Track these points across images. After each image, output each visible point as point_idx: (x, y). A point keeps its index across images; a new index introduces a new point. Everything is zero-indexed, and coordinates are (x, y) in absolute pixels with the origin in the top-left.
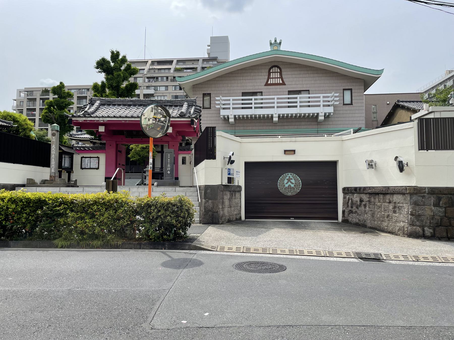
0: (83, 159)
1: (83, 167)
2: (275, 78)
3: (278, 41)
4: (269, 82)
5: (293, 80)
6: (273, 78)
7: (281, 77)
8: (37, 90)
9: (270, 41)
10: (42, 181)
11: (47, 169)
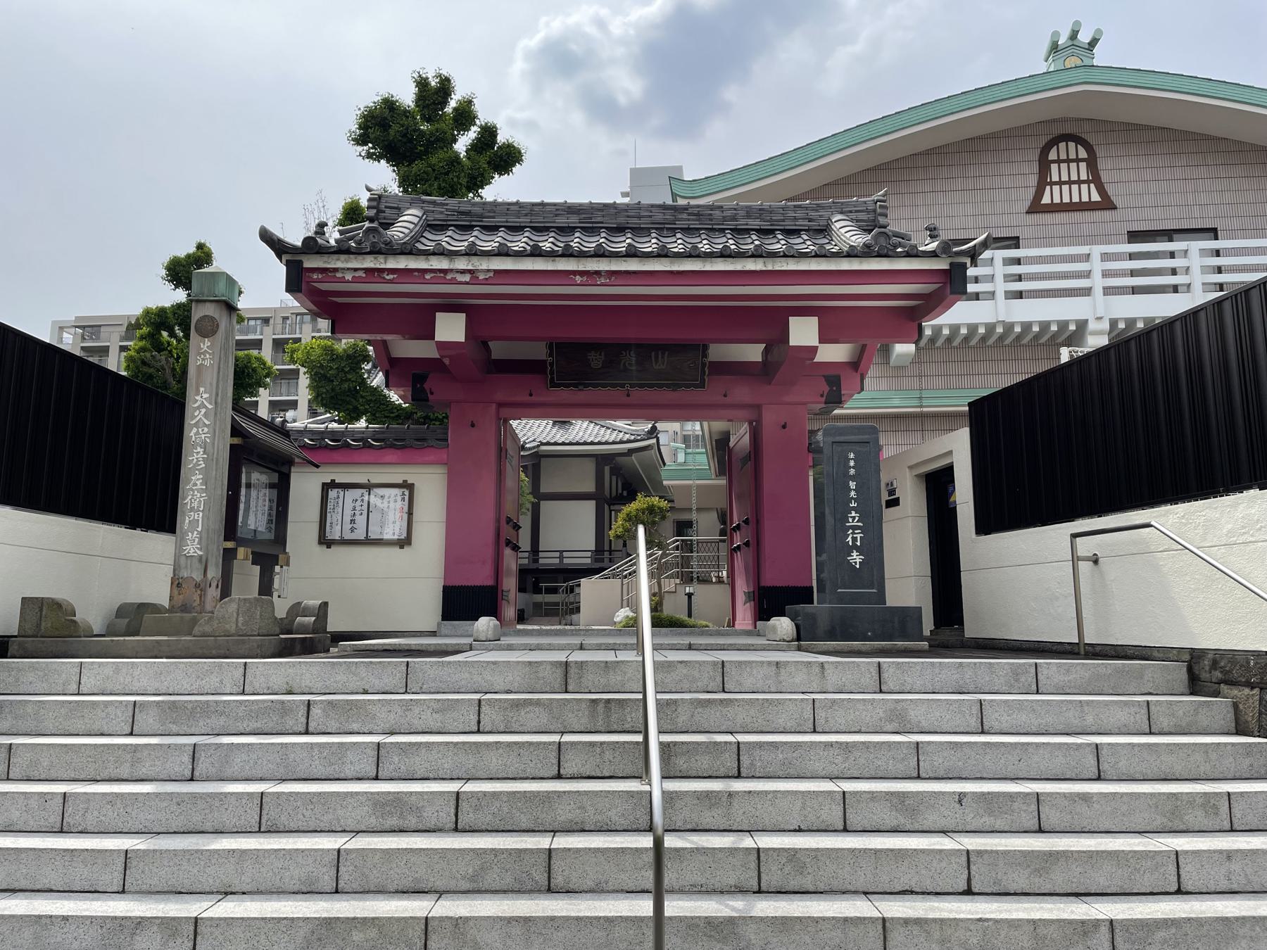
0: (333, 493)
1: (334, 533)
2: (1070, 183)
3: (1084, 37)
4: (1046, 200)
5: (1142, 189)
6: (1060, 183)
7: (1096, 179)
8: (111, 322)
9: (1056, 34)
10: (122, 611)
11: (154, 544)
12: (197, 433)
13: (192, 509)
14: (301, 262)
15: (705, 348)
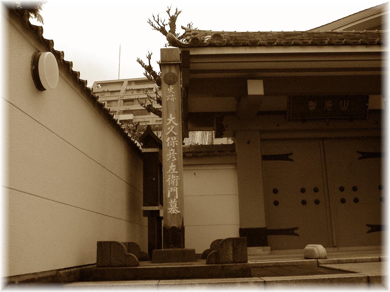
12: (170, 140)
13: (171, 186)
14: (189, 52)
15: (368, 97)
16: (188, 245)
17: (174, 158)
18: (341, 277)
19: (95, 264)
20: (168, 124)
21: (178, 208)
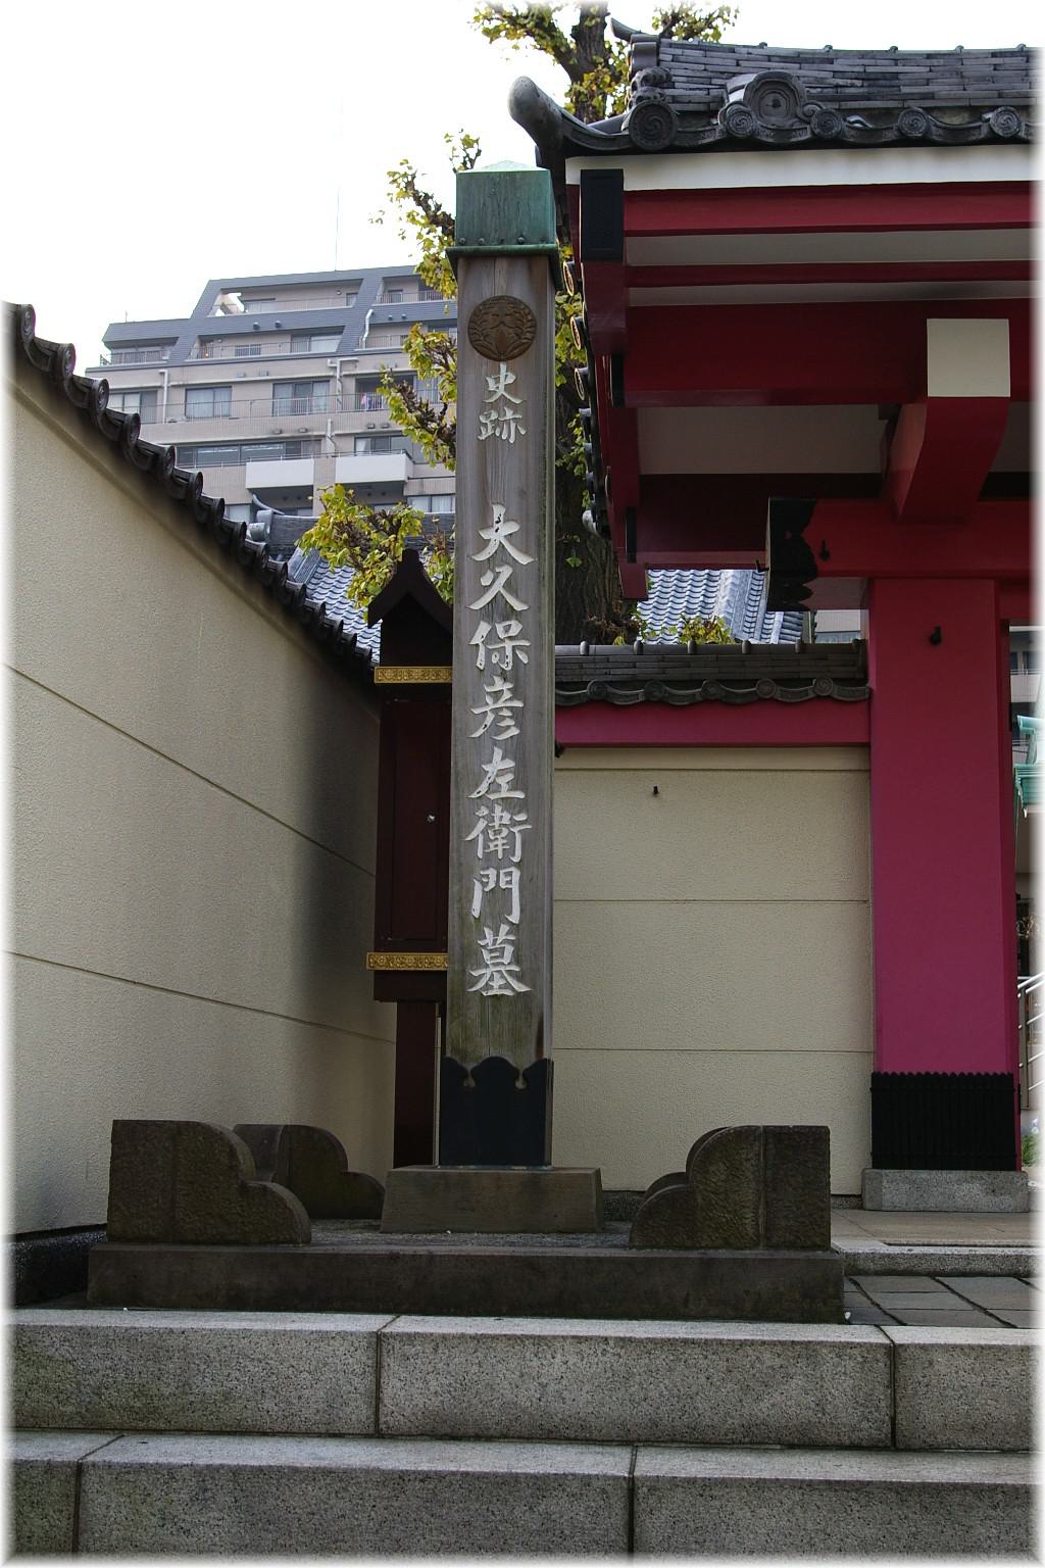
12: (492, 637)
13: (490, 859)
14: (618, 176)
16: (568, 1150)
17: (508, 727)
18: (994, 1343)
19: (103, 1227)
20: (482, 557)
21: (517, 969)
